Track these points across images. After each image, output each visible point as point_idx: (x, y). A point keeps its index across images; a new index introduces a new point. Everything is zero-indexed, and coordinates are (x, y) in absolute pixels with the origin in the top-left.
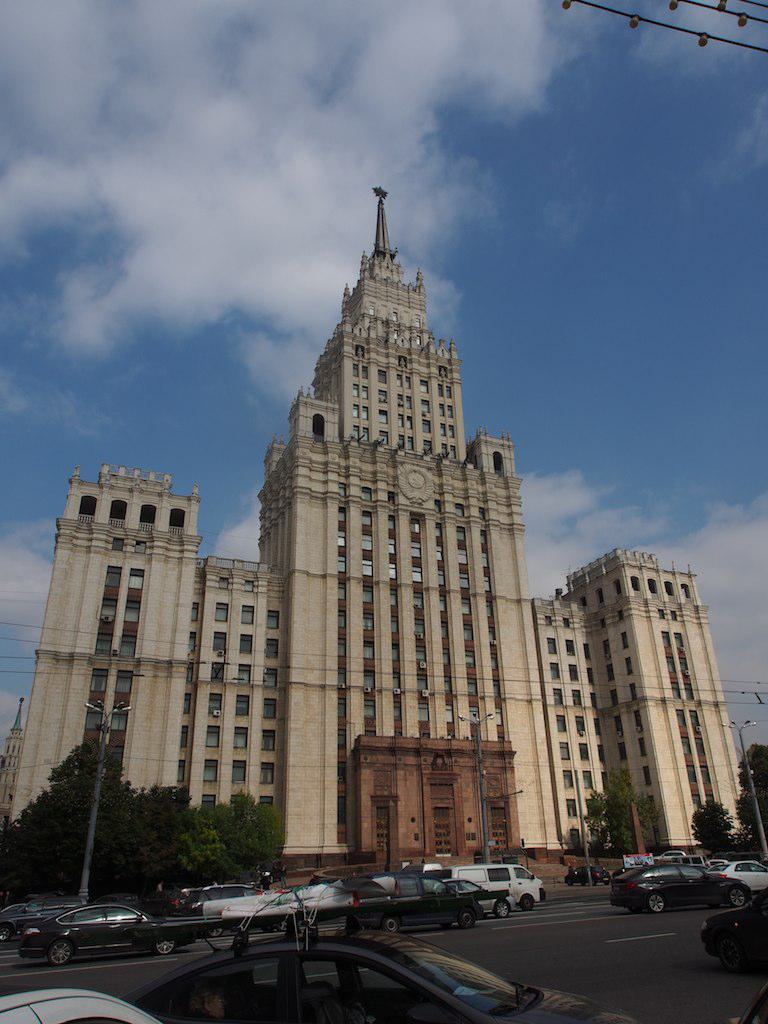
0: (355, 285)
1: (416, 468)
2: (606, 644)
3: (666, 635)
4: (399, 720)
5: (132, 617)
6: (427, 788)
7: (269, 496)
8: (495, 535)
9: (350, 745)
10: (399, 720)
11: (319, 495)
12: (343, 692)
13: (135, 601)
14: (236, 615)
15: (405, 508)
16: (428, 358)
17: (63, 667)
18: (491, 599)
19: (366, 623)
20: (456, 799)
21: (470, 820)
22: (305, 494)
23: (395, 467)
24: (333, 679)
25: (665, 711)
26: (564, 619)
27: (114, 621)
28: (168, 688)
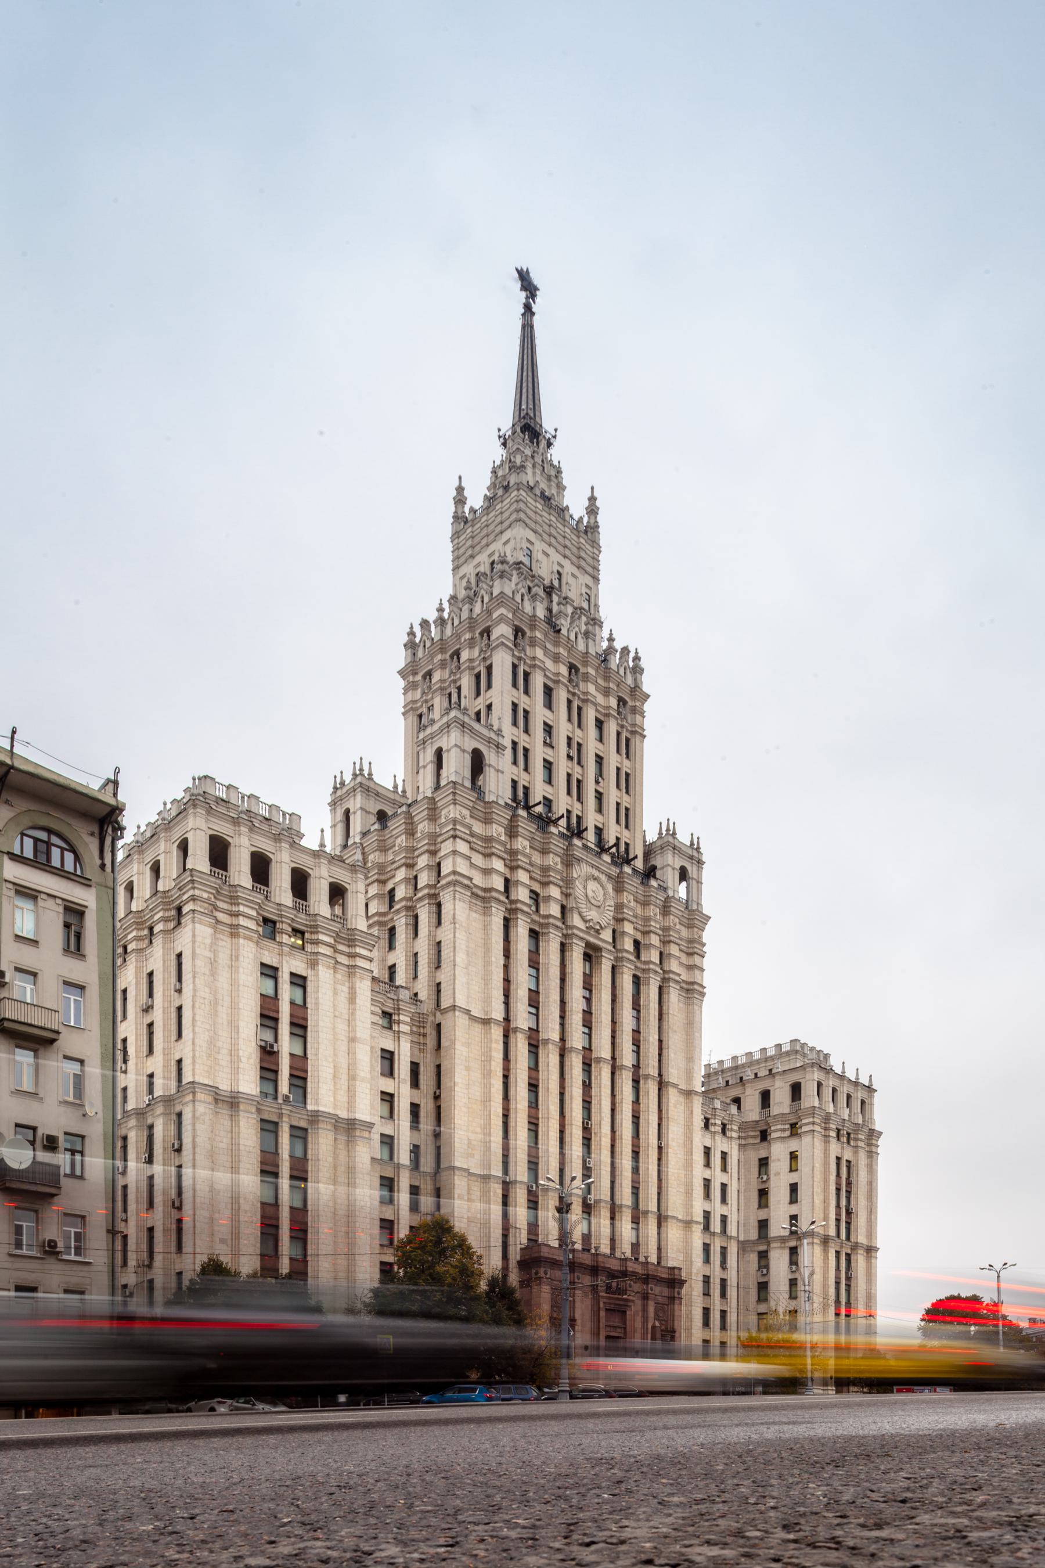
1: (596, 874)
6: (602, 1314)
8: (674, 997)
9: (515, 1255)
13: (300, 1027)
15: (582, 935)
16: (607, 678)
20: (628, 1329)
22: (467, 887)
24: (497, 1171)
26: (384, 1013)
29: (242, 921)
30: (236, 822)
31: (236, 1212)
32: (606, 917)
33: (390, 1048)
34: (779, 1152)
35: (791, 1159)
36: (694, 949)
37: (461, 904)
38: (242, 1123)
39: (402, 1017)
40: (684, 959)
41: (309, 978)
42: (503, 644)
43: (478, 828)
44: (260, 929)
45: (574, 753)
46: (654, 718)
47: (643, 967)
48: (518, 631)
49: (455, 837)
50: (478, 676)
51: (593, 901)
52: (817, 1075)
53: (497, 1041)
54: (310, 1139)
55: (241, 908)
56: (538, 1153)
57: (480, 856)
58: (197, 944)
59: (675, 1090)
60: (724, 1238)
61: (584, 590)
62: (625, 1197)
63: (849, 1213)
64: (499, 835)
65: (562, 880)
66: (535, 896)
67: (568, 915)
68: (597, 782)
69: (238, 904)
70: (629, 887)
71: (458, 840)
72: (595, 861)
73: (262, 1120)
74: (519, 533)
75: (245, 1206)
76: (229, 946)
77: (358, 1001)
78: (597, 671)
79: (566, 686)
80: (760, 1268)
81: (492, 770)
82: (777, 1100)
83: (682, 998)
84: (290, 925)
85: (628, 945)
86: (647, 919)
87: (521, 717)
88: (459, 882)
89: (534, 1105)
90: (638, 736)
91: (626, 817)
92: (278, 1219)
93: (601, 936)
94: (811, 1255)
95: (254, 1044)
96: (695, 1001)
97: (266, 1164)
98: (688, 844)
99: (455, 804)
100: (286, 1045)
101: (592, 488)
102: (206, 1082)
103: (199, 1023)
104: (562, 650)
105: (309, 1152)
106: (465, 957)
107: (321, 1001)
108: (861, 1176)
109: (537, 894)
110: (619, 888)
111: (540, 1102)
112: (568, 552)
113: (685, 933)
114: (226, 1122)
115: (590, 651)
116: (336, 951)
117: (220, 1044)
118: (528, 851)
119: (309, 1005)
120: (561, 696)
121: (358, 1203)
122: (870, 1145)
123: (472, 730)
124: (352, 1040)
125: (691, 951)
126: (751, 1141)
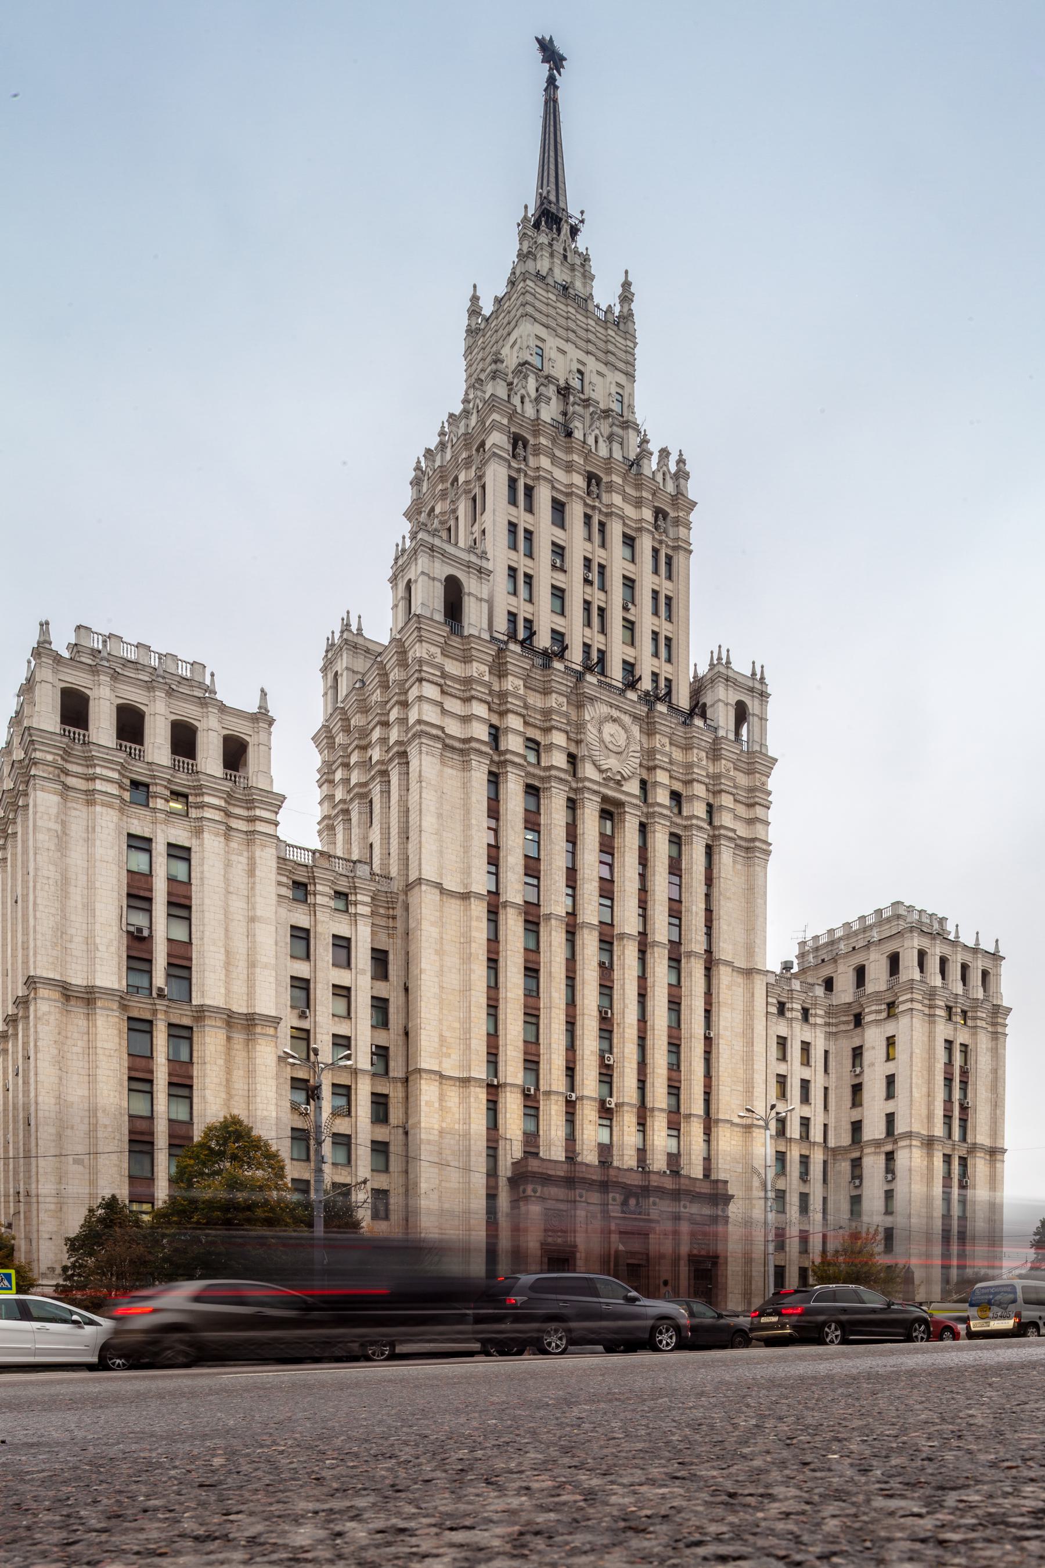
0: (501, 290)
1: (615, 713)
2: (857, 1053)
3: (949, 1044)
4: (571, 1139)
5: (179, 933)
7: (340, 738)
8: (726, 856)
9: (505, 1170)
10: (571, 1139)
11: (457, 745)
12: (494, 1090)
13: (181, 906)
14: (323, 951)
15: (596, 787)
16: (638, 487)
17: (78, 1010)
18: (710, 965)
19: (176, 1051)
21: (666, 1283)
22: (436, 738)
23: (580, 706)
24: (480, 1071)
25: (930, 1156)
27: (151, 936)
28: (250, 1058)
29: (99, 785)
30: (94, 670)
31: (93, 1130)
32: (631, 765)
33: (305, 924)
34: (873, 1038)
35: (888, 1046)
36: (755, 799)
37: (429, 758)
38: (99, 1023)
39: (359, 897)
40: (741, 810)
41: (193, 850)
42: (495, 454)
43: (453, 668)
44: (127, 796)
45: (594, 576)
46: (702, 530)
47: (685, 823)
48: (517, 440)
49: (420, 680)
50: (474, 499)
51: (611, 746)
52: (916, 942)
53: (478, 919)
54: (195, 1039)
55: (98, 770)
56: (538, 1050)
57: (459, 702)
58: (39, 815)
59: (729, 969)
60: (805, 1144)
61: (614, 389)
62: (659, 1096)
63: (964, 1108)
64: (481, 674)
65: (708, 776)
66: (676, 797)
67: (579, 765)
68: (625, 609)
69: (95, 766)
70: (663, 728)
71: (424, 683)
72: (616, 700)
73: (129, 1018)
74: (527, 330)
75: (103, 1119)
76: (85, 815)
77: (258, 873)
78: (624, 479)
79: (581, 498)
80: (853, 1178)
81: (472, 599)
82: (872, 976)
83: (739, 859)
84: (166, 787)
85: (662, 797)
86: (689, 766)
87: (520, 537)
88: (422, 732)
89: (532, 994)
90: (681, 552)
91: (667, 647)
92: (152, 1134)
93: (624, 789)
94: (911, 1159)
95: (115, 929)
96: (757, 861)
97: (136, 1070)
98: (749, 674)
99: (421, 641)
100: (162, 928)
101: (626, 272)
102: (51, 976)
103: (41, 908)
104: (576, 457)
105: (195, 1054)
106: (434, 820)
107: (206, 874)
108: (982, 1063)
109: (538, 743)
110: (650, 731)
111: (541, 990)
112: (591, 347)
113: (742, 780)
114: (80, 1023)
115: (615, 455)
116: (228, 814)
117: (73, 931)
118: (521, 692)
119: (193, 881)
120: (576, 511)
121: (259, 1113)
122: (994, 1024)
123: (444, 554)
124: (252, 920)
125: (752, 801)
126: (843, 1027)
